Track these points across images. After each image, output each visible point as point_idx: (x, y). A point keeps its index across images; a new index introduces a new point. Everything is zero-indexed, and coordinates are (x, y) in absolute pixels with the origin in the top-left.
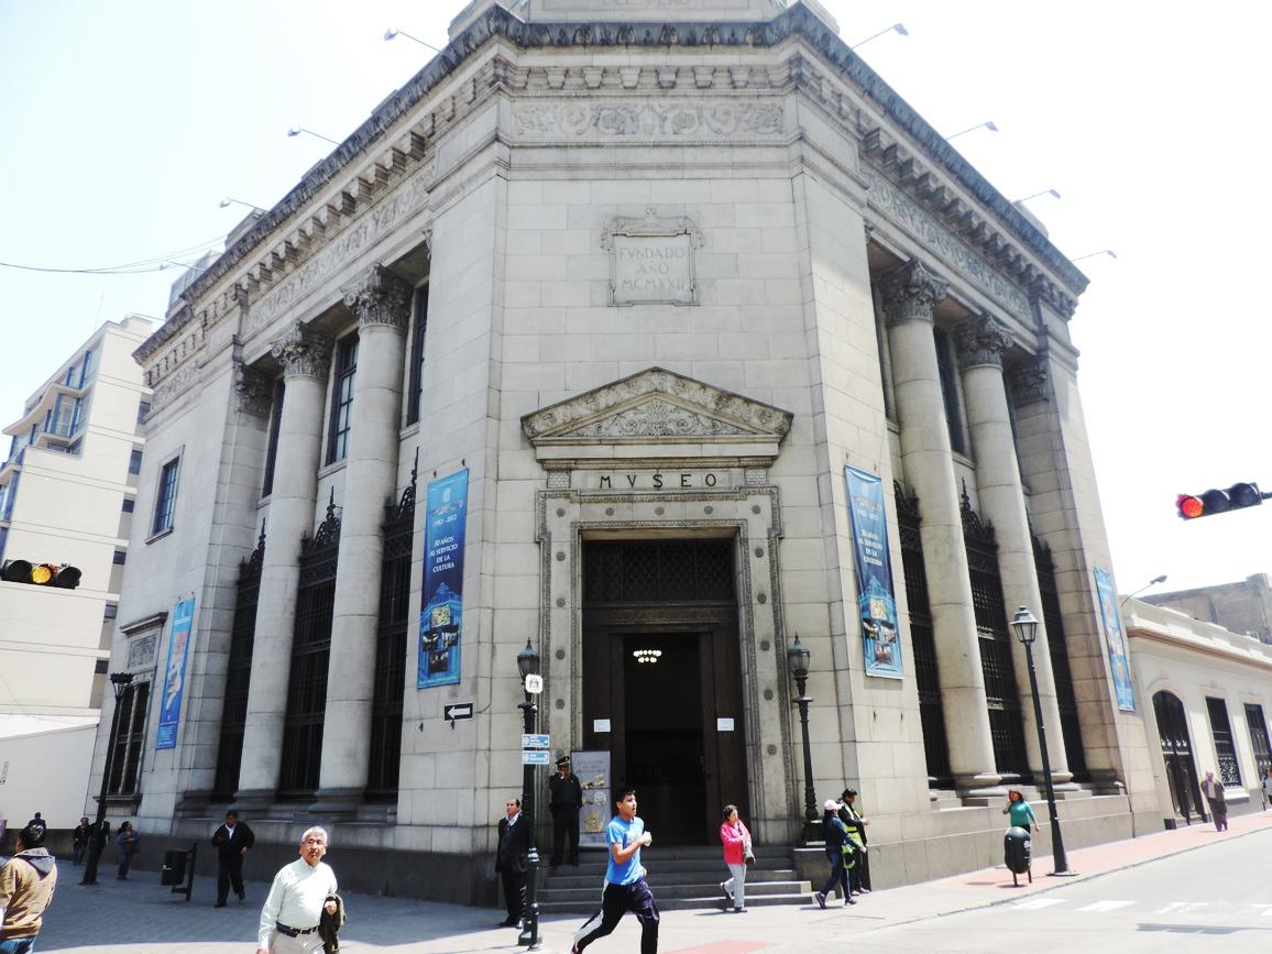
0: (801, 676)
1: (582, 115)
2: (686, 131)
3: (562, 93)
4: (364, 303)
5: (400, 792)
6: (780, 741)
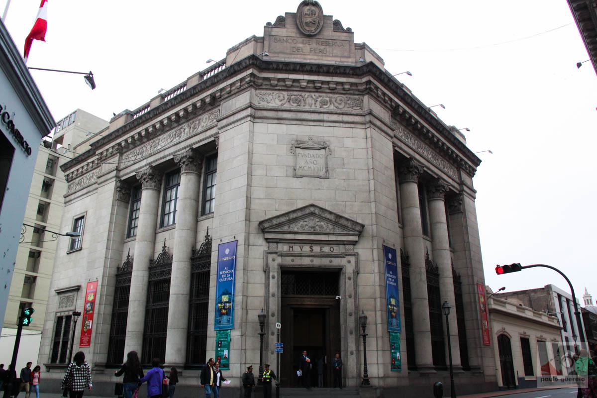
0: (364, 327)
1: (284, 97)
2: (325, 107)
3: (276, 88)
4: (144, 179)
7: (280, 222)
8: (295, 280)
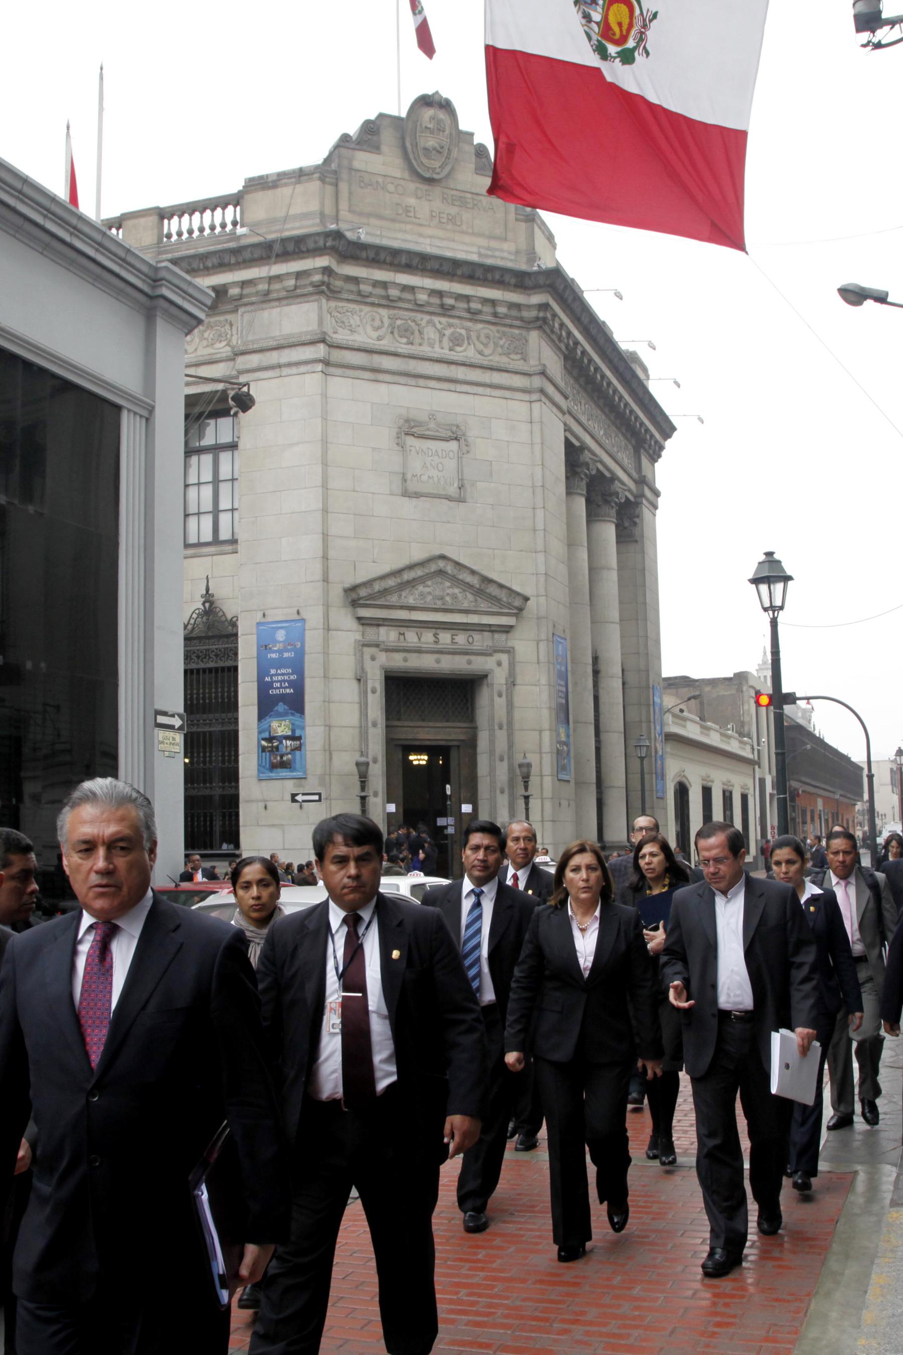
2: (458, 349)
7: (387, 587)
8: (407, 692)
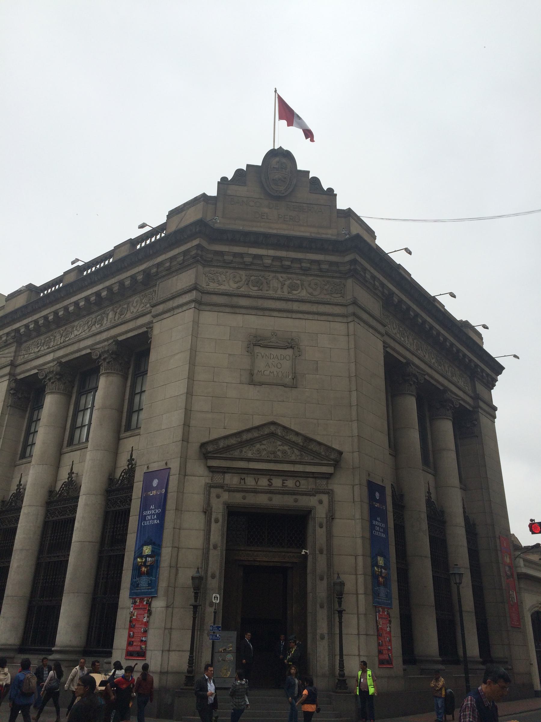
0: (340, 596)
2: (295, 292)
4: (104, 359)
5: (113, 651)
6: (327, 632)
